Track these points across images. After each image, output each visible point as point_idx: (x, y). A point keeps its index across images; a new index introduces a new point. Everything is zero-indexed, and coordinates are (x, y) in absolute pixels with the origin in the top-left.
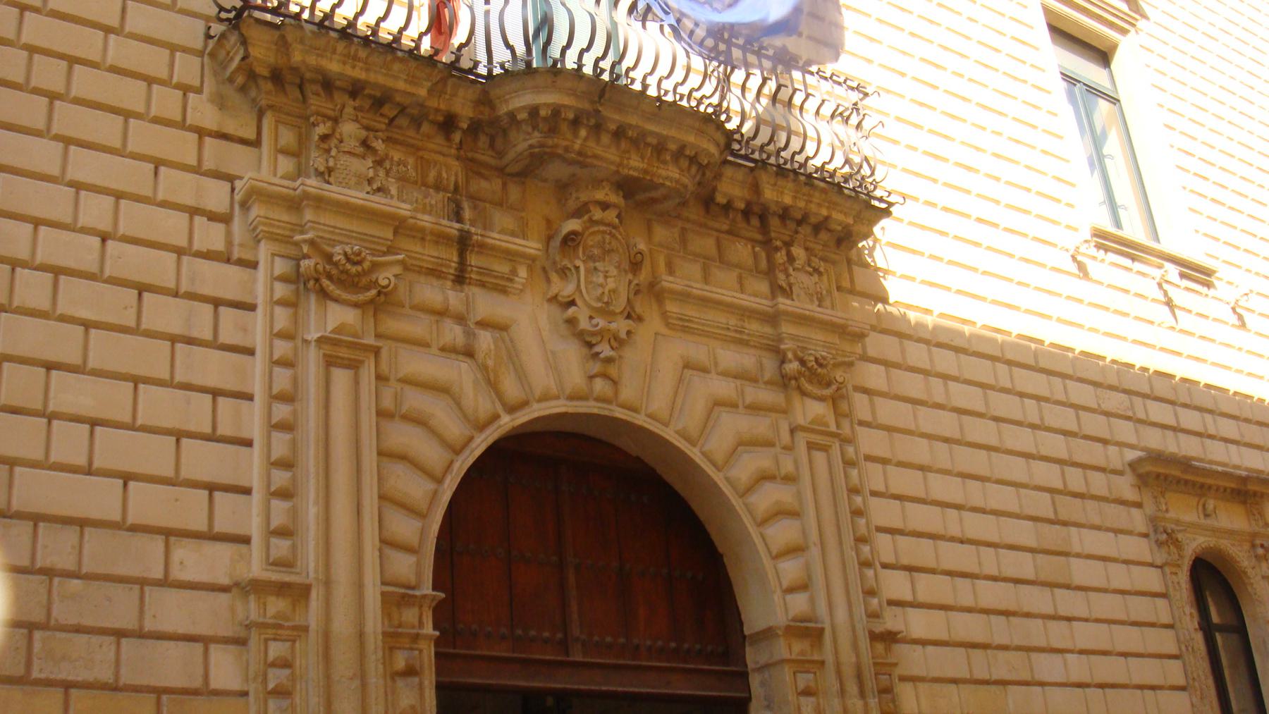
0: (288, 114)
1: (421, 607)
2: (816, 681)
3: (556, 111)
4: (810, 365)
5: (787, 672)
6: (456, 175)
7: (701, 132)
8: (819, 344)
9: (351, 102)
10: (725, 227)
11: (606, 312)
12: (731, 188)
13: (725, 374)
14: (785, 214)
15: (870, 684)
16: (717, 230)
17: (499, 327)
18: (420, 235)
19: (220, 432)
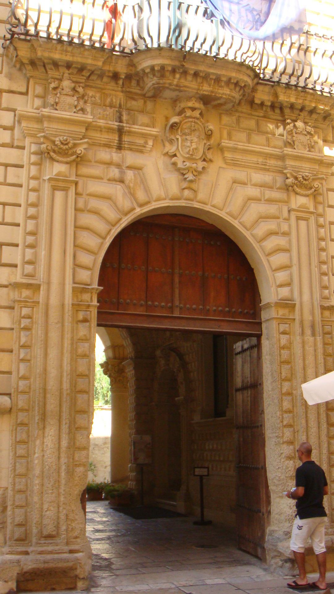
0: (40, 79)
1: (92, 293)
3: (163, 68)
4: (299, 179)
5: (274, 324)
7: (239, 71)
8: (306, 169)
9: (67, 71)
10: (262, 115)
11: (191, 158)
12: (263, 95)
13: (255, 185)
14: (292, 107)
15: (319, 329)
18: (100, 129)
19: (6, 221)
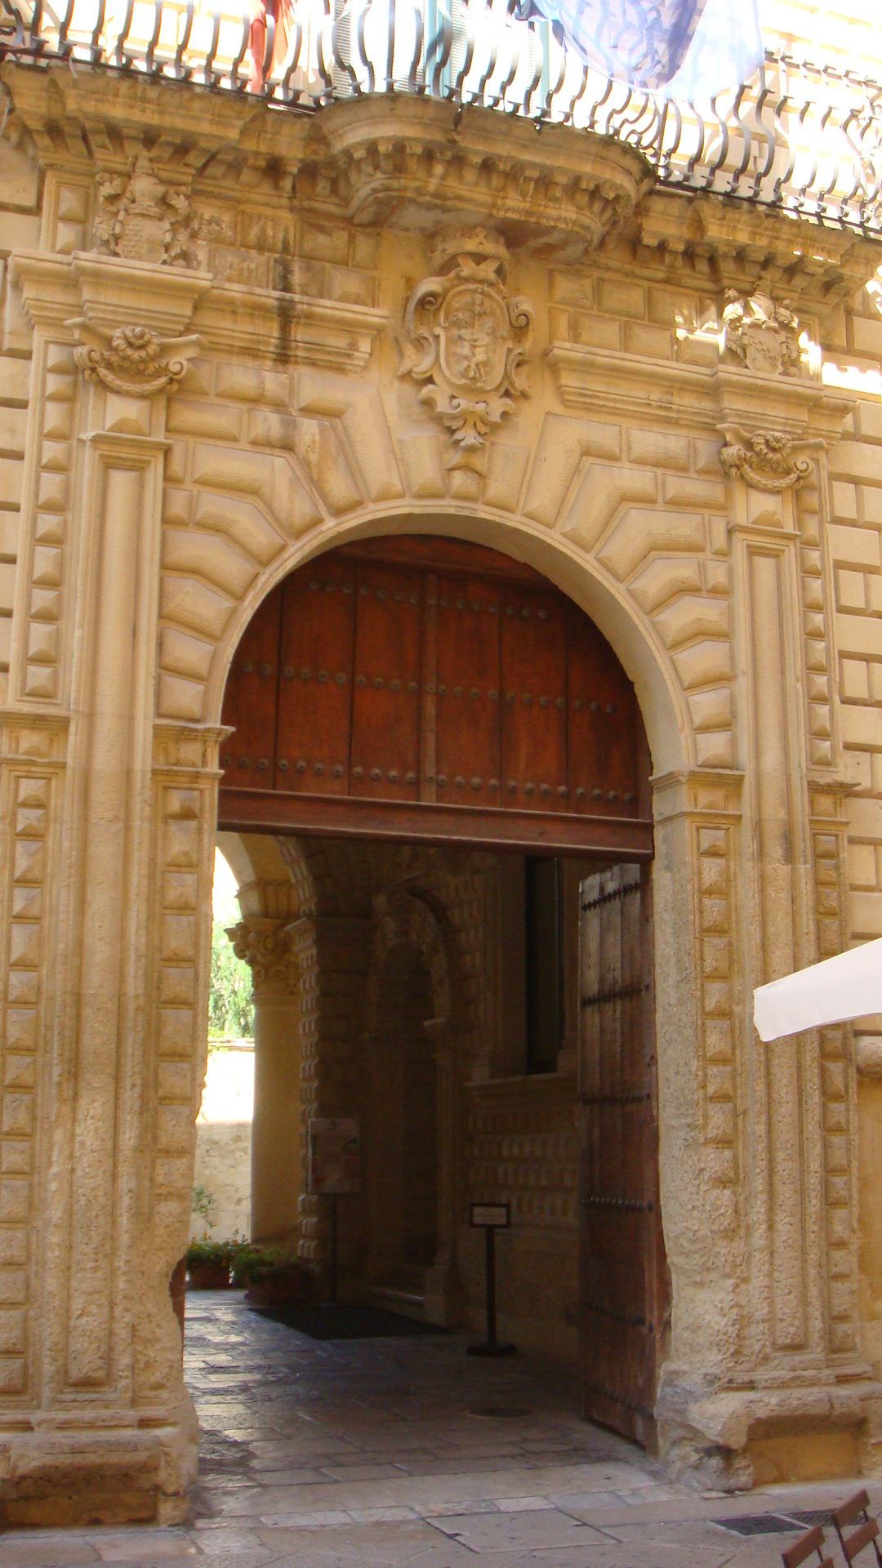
1: (205, 742)
2: (727, 841)
3: (399, 147)
6: (286, 231)
7: (600, 159)
9: (145, 153)
10: (660, 275)
11: (472, 389)
12: (664, 224)
13: (641, 462)
14: (741, 256)
15: (803, 844)
16: (649, 280)
17: (329, 414)
18: (230, 308)
